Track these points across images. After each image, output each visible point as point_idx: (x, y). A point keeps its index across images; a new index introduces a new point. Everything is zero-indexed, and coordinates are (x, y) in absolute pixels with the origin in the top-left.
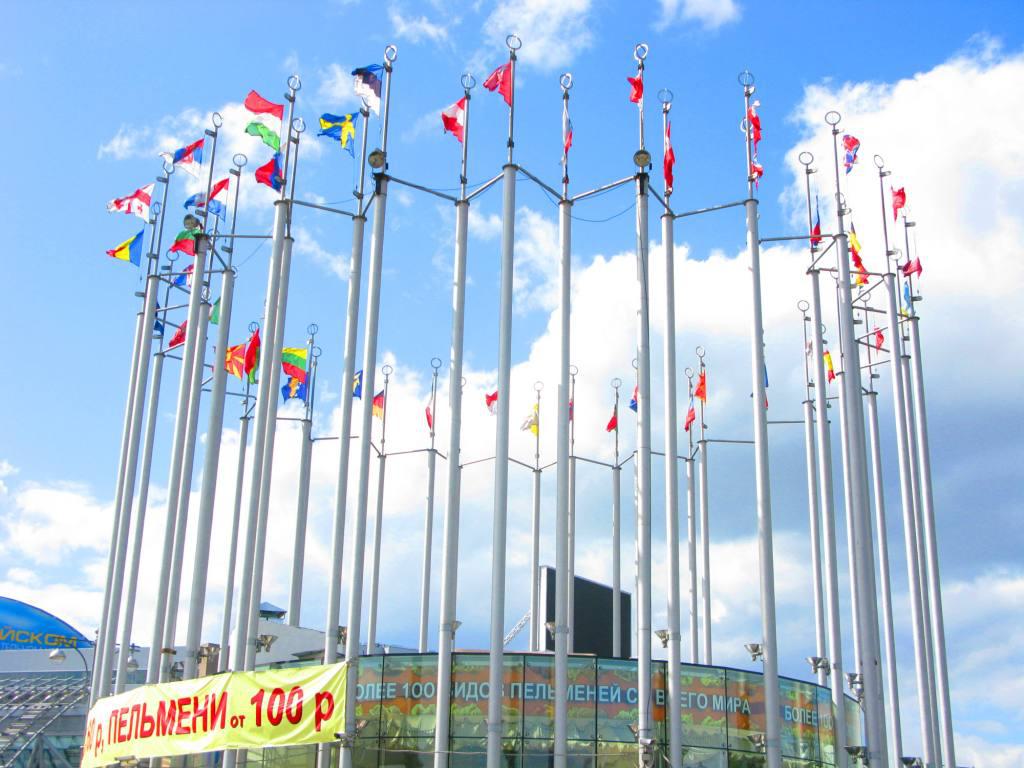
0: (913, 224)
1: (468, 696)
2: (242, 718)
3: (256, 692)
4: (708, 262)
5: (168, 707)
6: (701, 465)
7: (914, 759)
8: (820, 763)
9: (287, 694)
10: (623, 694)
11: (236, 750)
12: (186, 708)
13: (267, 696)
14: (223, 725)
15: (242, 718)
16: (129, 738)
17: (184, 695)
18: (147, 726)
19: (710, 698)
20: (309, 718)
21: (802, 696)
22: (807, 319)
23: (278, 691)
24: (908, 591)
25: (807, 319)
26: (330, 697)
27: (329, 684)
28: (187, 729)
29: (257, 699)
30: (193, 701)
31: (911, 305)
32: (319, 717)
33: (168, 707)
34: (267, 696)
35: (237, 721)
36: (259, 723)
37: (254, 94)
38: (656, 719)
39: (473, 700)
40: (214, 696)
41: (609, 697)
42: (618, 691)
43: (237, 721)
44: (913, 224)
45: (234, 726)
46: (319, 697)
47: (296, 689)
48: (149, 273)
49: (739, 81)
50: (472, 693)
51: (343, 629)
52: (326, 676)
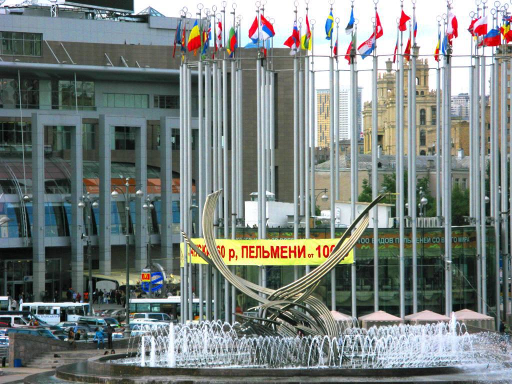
0: (231, 13)
1: (381, 243)
2: (312, 255)
3: (317, 246)
5: (275, 249)
6: (335, 134)
8: (8, 138)
10: (431, 240)
14: (305, 257)
15: (312, 255)
16: (256, 257)
18: (266, 254)
19: (458, 238)
23: (326, 246)
28: (286, 257)
29: (318, 248)
30: (288, 247)
31: (380, 88)
33: (275, 249)
35: (310, 256)
36: (319, 256)
38: (492, 259)
39: (383, 244)
40: (299, 247)
41: (426, 241)
42: (430, 239)
43: (310, 256)
44: (231, 13)
45: (310, 257)
48: (500, 209)
49: (197, 6)
50: (382, 241)
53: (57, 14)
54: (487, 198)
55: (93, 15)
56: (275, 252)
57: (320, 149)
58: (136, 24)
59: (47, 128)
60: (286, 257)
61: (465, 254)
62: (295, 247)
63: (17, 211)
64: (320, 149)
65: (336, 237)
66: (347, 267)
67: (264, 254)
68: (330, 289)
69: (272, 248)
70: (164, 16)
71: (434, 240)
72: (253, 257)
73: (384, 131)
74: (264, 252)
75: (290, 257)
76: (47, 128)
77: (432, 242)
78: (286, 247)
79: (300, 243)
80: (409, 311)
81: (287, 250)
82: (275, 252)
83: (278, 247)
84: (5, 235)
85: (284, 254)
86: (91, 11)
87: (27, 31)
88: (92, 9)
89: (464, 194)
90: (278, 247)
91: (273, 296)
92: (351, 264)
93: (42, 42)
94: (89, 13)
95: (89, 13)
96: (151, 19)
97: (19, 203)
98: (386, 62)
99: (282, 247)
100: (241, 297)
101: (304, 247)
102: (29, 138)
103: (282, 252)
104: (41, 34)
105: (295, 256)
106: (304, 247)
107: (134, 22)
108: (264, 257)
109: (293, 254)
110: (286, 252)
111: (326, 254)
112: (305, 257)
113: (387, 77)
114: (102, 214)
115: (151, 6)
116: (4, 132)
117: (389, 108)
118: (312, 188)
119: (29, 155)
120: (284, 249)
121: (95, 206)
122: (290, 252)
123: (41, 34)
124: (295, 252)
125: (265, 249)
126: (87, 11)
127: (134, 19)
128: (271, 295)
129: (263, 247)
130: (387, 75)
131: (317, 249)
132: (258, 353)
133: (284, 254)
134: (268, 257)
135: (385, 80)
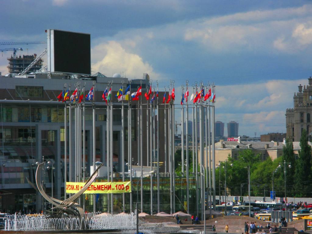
3: (116, 185)
4: (244, 135)
5: (99, 186)
7: (174, 100)
9: (121, 186)
11: (111, 194)
12: (102, 187)
13: (118, 186)
14: (111, 190)
16: (91, 190)
17: (103, 185)
18: (95, 189)
20: (125, 189)
21: (305, 183)
22: (194, 88)
23: (119, 185)
24: (64, 158)
25: (194, 88)
26: (128, 186)
27: (128, 184)
28: (103, 190)
29: (117, 186)
32: (127, 189)
33: (99, 186)
34: (118, 186)
36: (117, 189)
37: (104, 120)
46: (127, 186)
47: (123, 185)
51: (110, 178)
52: (128, 183)
53: (51, 77)
54: (82, 168)
55: (70, 77)
56: (99, 188)
57: (282, 134)
58: (89, 81)
59: (42, 131)
60: (103, 190)
61: (182, 188)
62: (107, 186)
63: (29, 171)
64: (282, 134)
65: (85, 182)
66: (129, 194)
67: (95, 189)
68: (123, 204)
69: (98, 186)
70: (106, 77)
71: (168, 182)
72: (90, 190)
73: (294, 126)
74: (94, 188)
75: (105, 190)
76: (42, 131)
77: (167, 183)
78: (103, 186)
79: (108, 184)
80: (155, 212)
81: (104, 186)
82: (99, 188)
83: (100, 186)
84: (22, 182)
85: (103, 189)
86: (69, 75)
87: (35, 85)
88: (69, 74)
89: (273, 162)
90: (100, 186)
91: (62, 203)
92: (130, 193)
93: (43, 91)
94: (68, 76)
95: (68, 76)
96: (98, 79)
97: (30, 167)
98: (299, 87)
99: (102, 186)
100: (88, 207)
101: (110, 186)
102: (34, 136)
103: (102, 188)
104: (43, 87)
105: (107, 190)
106: (110, 186)
107: (90, 80)
108: (94, 190)
109: (106, 189)
110: (103, 188)
111: (120, 188)
112: (111, 190)
113: (299, 95)
114: (57, 173)
115: (99, 72)
116: (24, 134)
117: (295, 113)
118: (209, 160)
119: (35, 144)
120: (102, 187)
121: (48, 168)
122: (105, 187)
123: (43, 87)
124: (107, 187)
125: (95, 187)
126: (67, 75)
127: (89, 79)
128: (61, 203)
129: (94, 186)
130: (299, 94)
131: (116, 186)
132: (52, 224)
133: (103, 189)
134: (96, 190)
135: (298, 97)
